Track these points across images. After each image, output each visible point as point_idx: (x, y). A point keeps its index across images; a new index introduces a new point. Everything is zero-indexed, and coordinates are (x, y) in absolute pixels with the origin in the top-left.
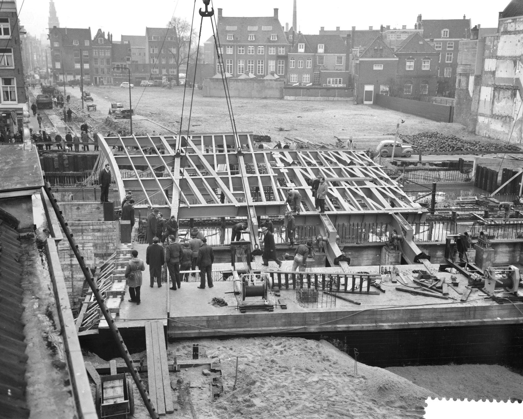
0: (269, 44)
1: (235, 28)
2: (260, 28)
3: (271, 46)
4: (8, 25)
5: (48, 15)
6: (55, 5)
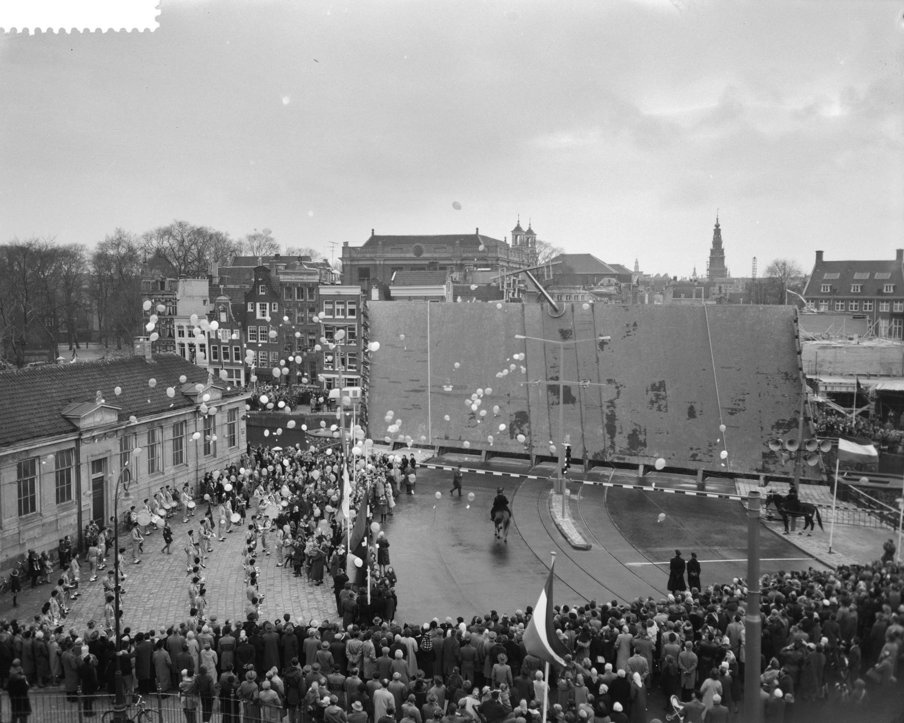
0: (880, 297)
2: (872, 275)
3: (883, 301)
5: (711, 246)
6: (722, 233)
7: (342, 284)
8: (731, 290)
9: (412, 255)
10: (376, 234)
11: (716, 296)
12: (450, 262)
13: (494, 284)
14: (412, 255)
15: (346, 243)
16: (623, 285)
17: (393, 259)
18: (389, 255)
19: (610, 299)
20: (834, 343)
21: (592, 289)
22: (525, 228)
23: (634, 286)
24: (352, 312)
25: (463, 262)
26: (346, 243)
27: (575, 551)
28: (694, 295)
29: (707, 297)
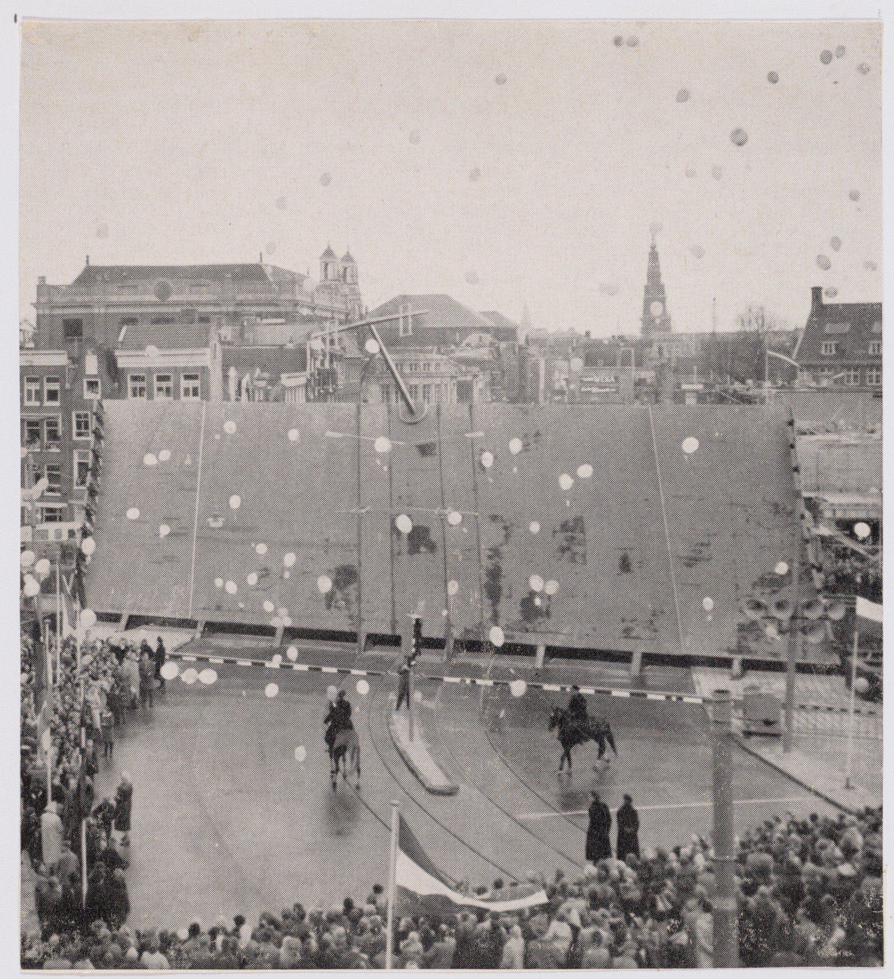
1: (846, 328)
4: (196, 383)
7: (37, 348)
8: (678, 352)
9: (154, 298)
10: (91, 263)
11: (654, 363)
12: (217, 309)
13: (290, 346)
14: (154, 298)
15: (42, 279)
16: (503, 345)
17: (127, 305)
18: (114, 298)
19: (483, 370)
20: (845, 439)
21: (452, 351)
22: (340, 253)
23: (520, 348)
24: (53, 395)
25: (239, 309)
26: (42, 279)
27: (431, 797)
28: (619, 362)
29: (639, 364)
